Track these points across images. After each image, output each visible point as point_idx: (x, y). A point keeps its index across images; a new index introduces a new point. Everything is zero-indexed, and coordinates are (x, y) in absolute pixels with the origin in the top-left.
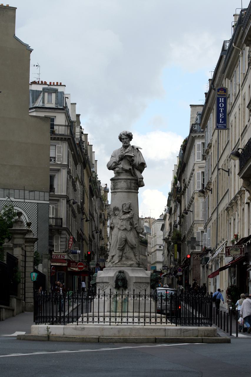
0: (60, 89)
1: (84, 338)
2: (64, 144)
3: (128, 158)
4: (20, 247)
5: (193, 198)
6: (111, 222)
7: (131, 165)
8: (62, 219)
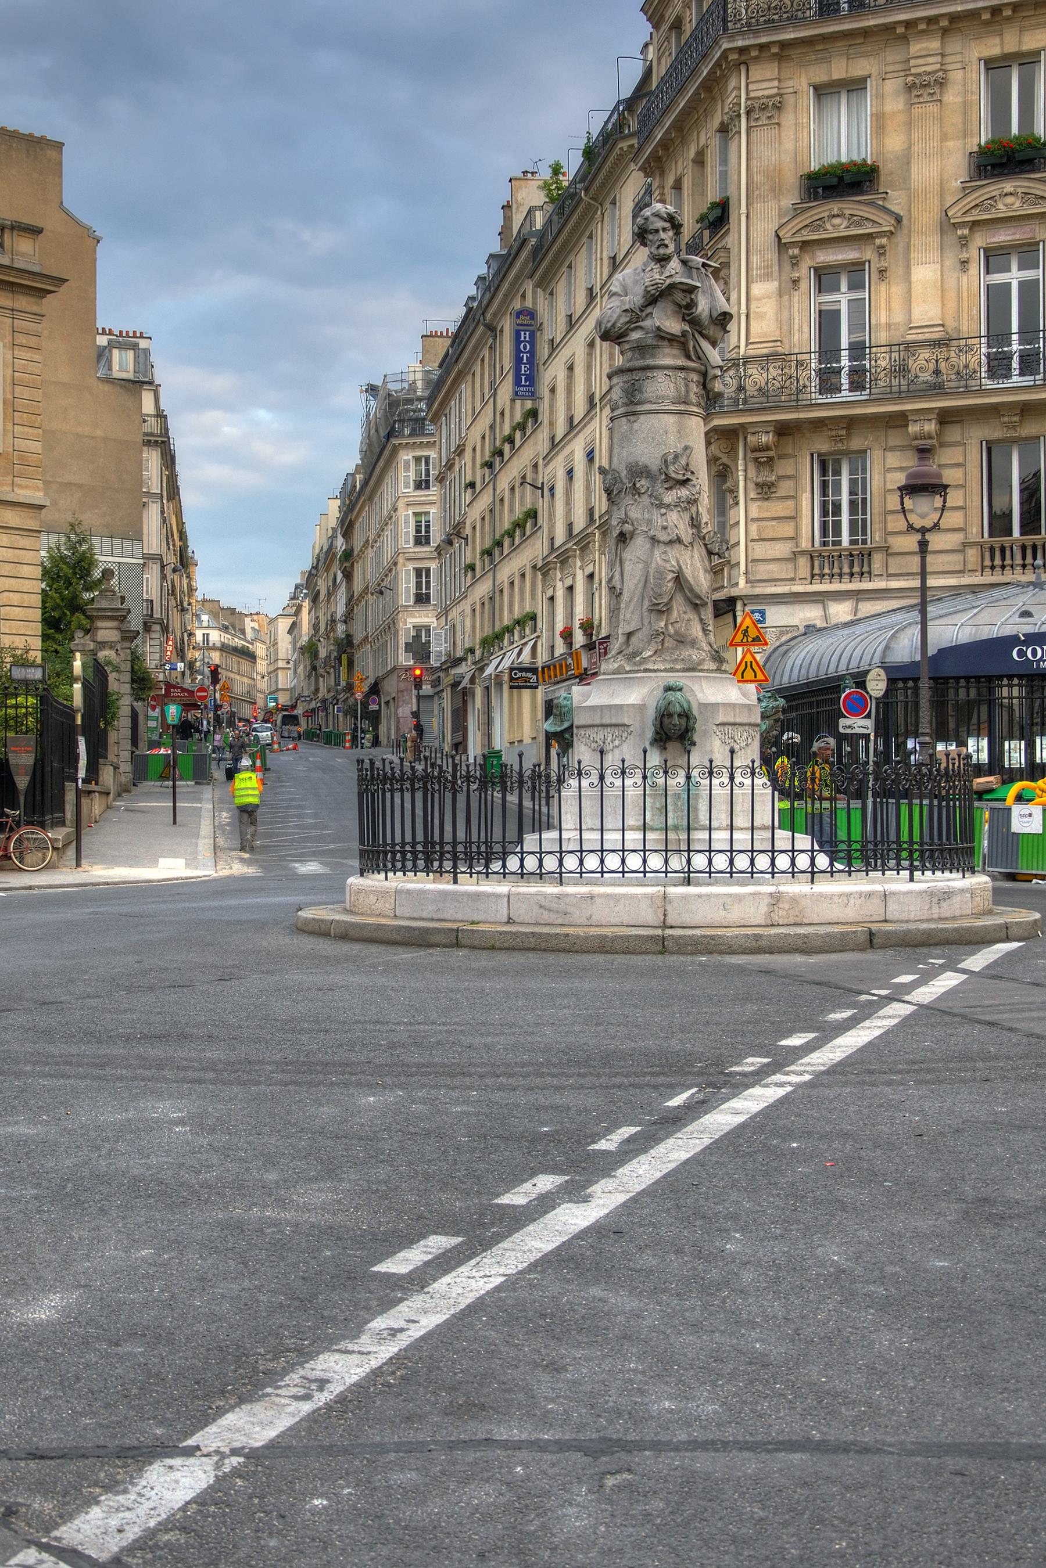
0: (143, 344)
1: (607, 937)
2: (154, 452)
3: (679, 296)
4: (111, 648)
5: (395, 564)
6: (623, 516)
7: (684, 320)
8: (152, 601)
